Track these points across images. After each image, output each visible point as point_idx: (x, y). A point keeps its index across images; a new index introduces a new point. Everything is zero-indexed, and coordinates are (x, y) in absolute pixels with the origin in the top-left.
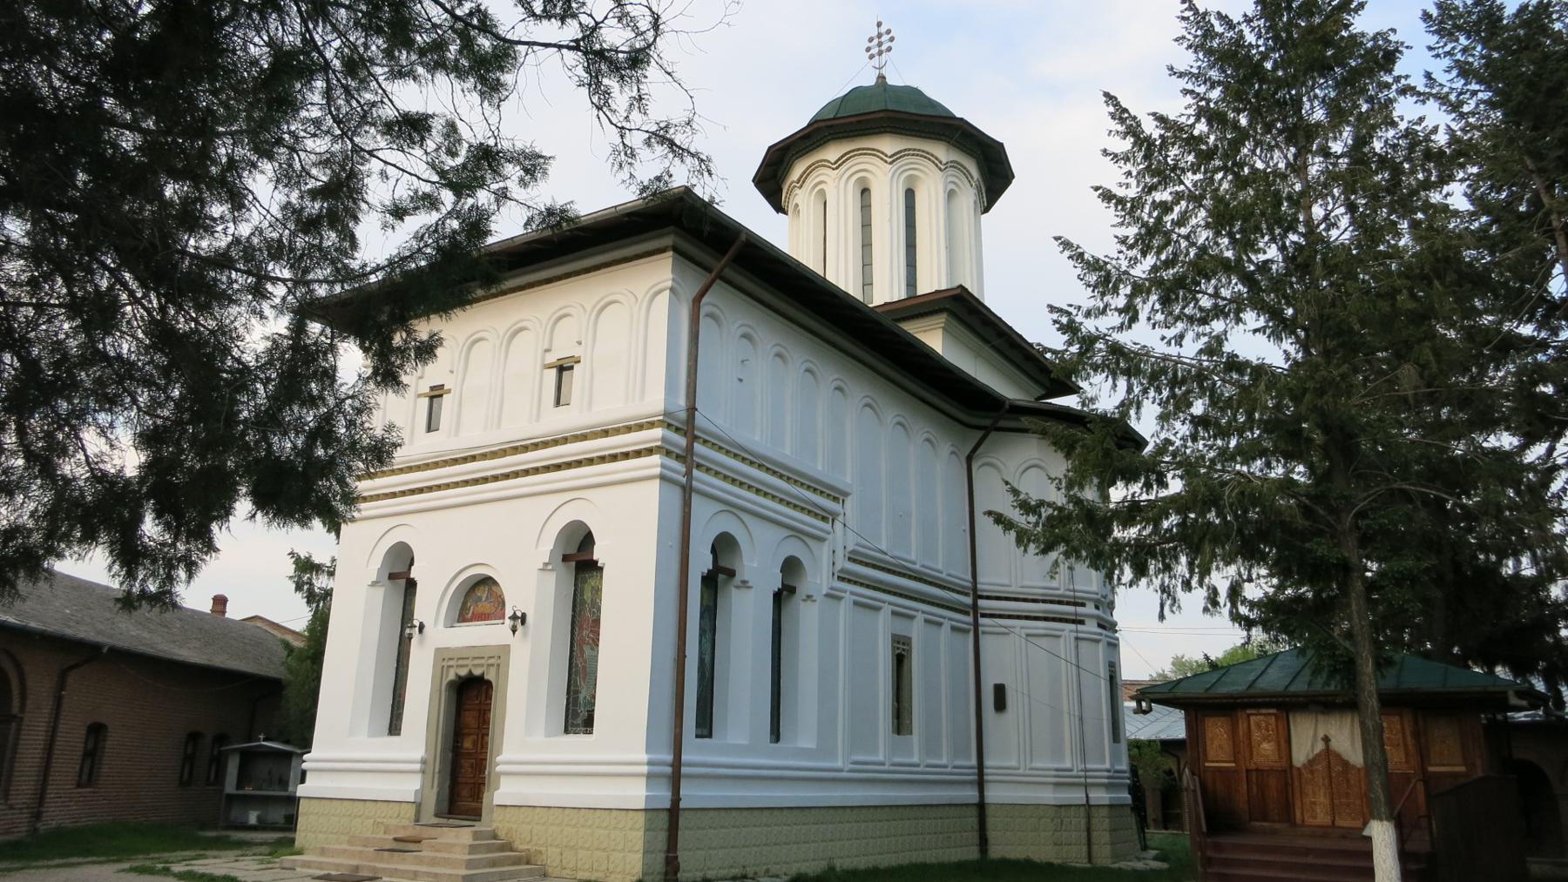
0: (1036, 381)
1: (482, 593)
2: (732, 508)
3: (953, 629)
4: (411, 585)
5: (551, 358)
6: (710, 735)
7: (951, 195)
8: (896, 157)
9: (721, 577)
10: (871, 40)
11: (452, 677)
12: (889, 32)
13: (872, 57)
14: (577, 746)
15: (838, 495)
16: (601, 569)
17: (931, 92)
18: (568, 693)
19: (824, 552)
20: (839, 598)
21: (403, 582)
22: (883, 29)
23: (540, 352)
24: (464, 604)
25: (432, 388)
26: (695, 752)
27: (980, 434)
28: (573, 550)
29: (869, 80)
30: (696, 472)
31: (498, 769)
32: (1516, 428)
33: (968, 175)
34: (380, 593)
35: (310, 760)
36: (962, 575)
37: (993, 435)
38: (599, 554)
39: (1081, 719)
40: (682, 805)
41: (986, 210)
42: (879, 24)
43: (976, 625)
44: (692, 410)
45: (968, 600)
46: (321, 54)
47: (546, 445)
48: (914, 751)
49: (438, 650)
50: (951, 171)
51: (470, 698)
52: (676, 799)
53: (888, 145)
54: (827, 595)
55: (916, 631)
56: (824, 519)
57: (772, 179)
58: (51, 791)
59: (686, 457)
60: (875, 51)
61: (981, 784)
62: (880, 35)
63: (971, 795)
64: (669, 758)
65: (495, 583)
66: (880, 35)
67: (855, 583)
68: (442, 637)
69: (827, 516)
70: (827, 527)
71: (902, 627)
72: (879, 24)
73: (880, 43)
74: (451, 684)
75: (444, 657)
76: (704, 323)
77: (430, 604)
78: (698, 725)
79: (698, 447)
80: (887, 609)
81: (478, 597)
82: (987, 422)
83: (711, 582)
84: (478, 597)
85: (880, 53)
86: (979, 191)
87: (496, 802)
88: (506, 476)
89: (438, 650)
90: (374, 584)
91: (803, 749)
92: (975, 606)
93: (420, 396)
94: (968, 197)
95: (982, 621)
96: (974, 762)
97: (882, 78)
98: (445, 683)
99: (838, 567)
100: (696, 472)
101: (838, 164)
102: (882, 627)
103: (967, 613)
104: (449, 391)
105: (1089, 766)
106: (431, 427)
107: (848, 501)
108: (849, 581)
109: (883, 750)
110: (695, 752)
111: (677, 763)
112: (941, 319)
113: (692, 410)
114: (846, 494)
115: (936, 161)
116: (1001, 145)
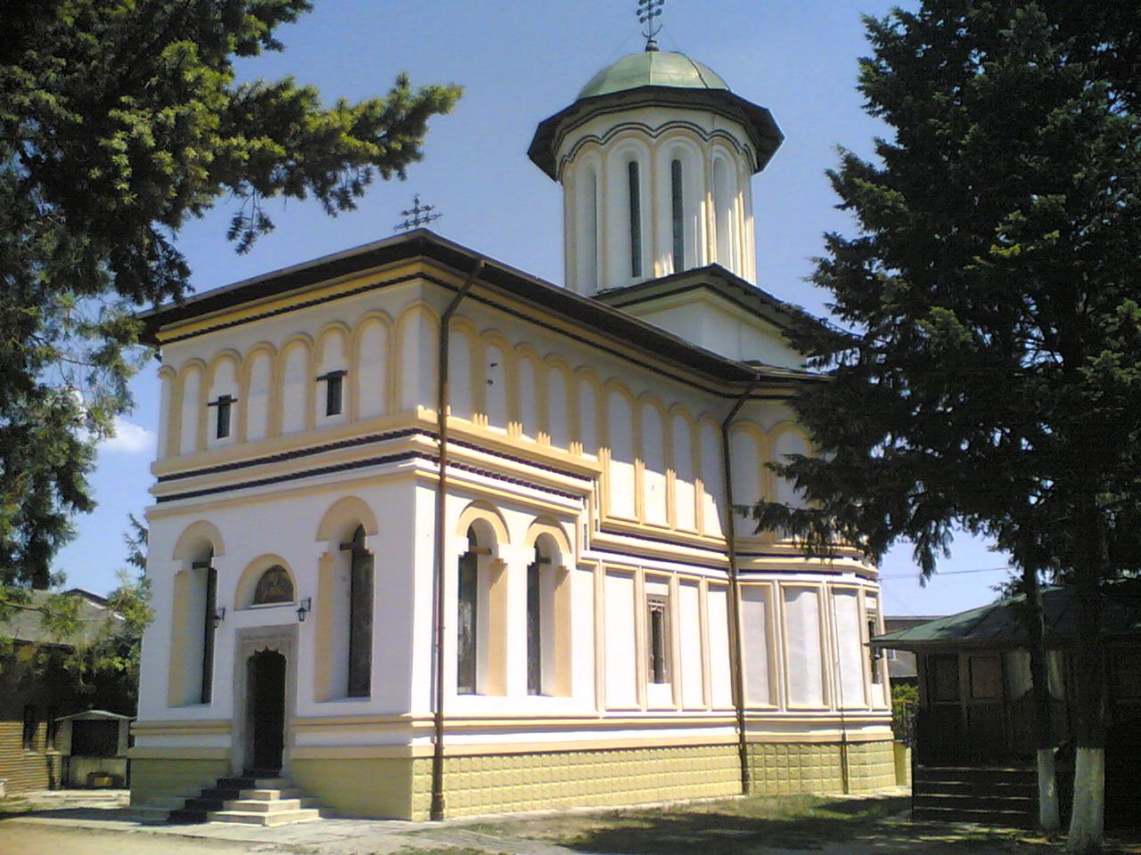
2: (482, 500)
4: (212, 575)
5: (323, 371)
13: (642, 20)
14: (658, 695)
21: (204, 570)
26: (457, 705)
27: (733, 402)
32: (882, 282)
38: (369, 543)
40: (445, 753)
46: (871, 274)
51: (267, 673)
52: (438, 747)
58: (747, 304)
60: (645, 14)
65: (284, 570)
68: (242, 621)
70: (578, 504)
74: (251, 659)
75: (244, 636)
77: (225, 594)
78: (459, 684)
79: (450, 447)
81: (273, 585)
83: (468, 563)
84: (273, 585)
85: (650, 16)
100: (449, 470)
106: (222, 431)
116: (765, 111)
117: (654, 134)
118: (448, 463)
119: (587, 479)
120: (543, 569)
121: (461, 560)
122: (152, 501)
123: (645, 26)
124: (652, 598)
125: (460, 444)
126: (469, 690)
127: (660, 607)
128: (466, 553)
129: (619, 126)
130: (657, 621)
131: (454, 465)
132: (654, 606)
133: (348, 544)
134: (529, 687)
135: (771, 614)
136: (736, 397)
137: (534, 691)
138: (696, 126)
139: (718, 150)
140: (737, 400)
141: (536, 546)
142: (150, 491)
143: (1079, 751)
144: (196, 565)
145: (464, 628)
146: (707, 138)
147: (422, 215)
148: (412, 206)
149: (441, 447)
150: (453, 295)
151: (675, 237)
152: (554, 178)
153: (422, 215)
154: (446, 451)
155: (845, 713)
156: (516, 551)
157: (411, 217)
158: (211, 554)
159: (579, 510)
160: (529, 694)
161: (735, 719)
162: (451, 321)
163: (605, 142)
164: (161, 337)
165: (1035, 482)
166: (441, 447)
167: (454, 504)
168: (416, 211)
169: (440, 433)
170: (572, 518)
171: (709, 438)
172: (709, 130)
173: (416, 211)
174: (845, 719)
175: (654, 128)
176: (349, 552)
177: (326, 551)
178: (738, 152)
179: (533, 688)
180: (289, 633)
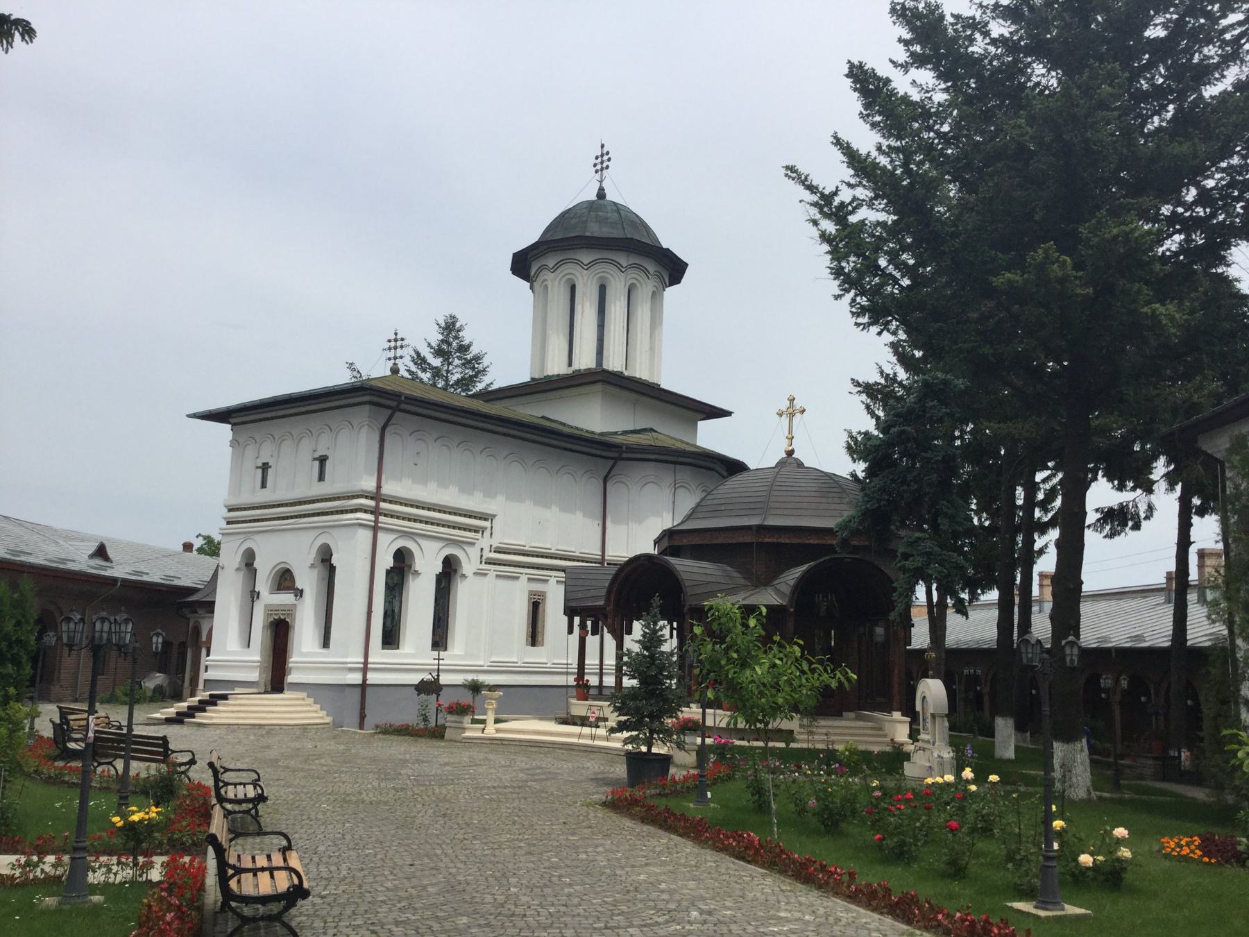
5: (317, 455)
19: (474, 552)
26: (379, 655)
27: (611, 462)
33: (646, 271)
37: (620, 463)
38: (334, 561)
42: (603, 146)
44: (379, 487)
48: (538, 656)
50: (632, 271)
52: (365, 679)
53: (586, 257)
54: (475, 574)
59: (376, 512)
62: (602, 155)
63: (356, 678)
66: (602, 155)
68: (270, 599)
70: (478, 536)
72: (603, 146)
75: (269, 609)
76: (387, 441)
77: (263, 585)
81: (285, 580)
82: (616, 455)
85: (602, 169)
88: (296, 517)
90: (238, 569)
97: (601, 194)
100: (381, 519)
111: (366, 663)
113: (379, 487)
114: (495, 516)
115: (618, 266)
118: (380, 514)
119: (486, 519)
121: (388, 572)
123: (598, 176)
124: (532, 593)
131: (386, 515)
139: (634, 275)
143: (1055, 744)
144: (323, 561)
147: (399, 343)
148: (393, 337)
150: (389, 412)
153: (399, 343)
156: (428, 563)
157: (393, 344)
165: (969, 504)
166: (377, 505)
168: (396, 340)
169: (377, 496)
171: (597, 485)
173: (396, 340)
180: (291, 610)
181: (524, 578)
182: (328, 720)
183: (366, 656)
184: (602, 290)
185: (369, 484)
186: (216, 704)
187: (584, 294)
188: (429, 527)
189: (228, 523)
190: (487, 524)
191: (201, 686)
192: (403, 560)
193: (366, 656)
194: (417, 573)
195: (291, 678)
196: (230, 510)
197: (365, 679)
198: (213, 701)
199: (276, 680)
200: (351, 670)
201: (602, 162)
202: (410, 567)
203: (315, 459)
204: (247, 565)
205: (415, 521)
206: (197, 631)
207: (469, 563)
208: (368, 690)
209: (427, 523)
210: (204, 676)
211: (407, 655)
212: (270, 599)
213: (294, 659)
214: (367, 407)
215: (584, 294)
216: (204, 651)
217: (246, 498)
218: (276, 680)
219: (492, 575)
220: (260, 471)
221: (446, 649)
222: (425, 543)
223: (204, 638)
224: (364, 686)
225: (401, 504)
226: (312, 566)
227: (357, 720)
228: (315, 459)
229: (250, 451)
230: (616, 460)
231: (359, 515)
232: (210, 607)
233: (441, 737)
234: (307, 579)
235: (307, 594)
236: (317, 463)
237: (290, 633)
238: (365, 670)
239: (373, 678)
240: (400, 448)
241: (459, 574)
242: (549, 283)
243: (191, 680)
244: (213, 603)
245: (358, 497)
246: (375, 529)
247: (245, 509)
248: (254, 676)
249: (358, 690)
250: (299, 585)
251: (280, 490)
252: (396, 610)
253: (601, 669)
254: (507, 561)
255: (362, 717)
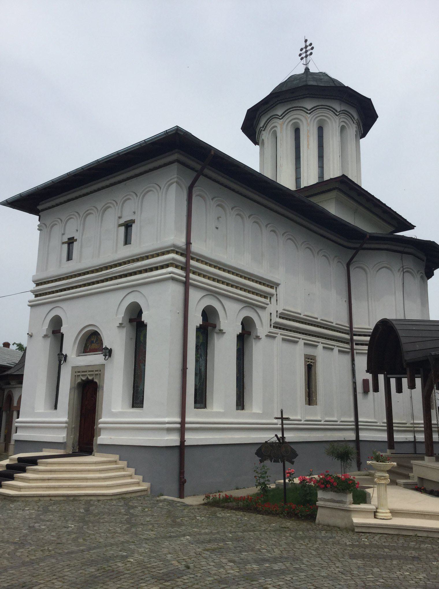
0: (389, 223)
1: (94, 339)
3: (340, 351)
5: (122, 221)
6: (243, 409)
7: (343, 129)
8: (314, 109)
9: (209, 328)
10: (301, 50)
11: (79, 381)
12: (311, 44)
13: (302, 59)
14: (136, 416)
15: (273, 285)
16: (146, 326)
17: (333, 75)
18: (134, 388)
19: (265, 315)
20: (274, 337)
22: (308, 43)
23: (117, 218)
24: (86, 345)
25: (69, 239)
26: (193, 416)
27: (354, 251)
28: (135, 316)
29: (300, 70)
30: (191, 275)
31: (100, 426)
33: (352, 117)
34: (49, 341)
35: (17, 422)
36: (345, 323)
38: (145, 318)
39: (411, 397)
40: (186, 444)
41: (363, 135)
42: (306, 41)
43: (352, 349)
44: (188, 243)
45: (348, 337)
47: (120, 264)
49: (72, 367)
50: (342, 116)
52: (183, 440)
54: (267, 336)
55: (319, 352)
56: (265, 297)
57: (253, 124)
59: (186, 268)
61: (357, 430)
62: (306, 47)
63: (173, 440)
64: (179, 420)
65: (99, 334)
66: (306, 47)
67: (283, 329)
68: (77, 360)
69: (265, 295)
70: (267, 301)
71: (310, 351)
72: (306, 41)
73: (307, 51)
74: (79, 384)
75: (76, 371)
77: (70, 347)
79: (192, 262)
80: (301, 342)
81: (92, 341)
82: (358, 245)
85: (306, 56)
86: (358, 125)
87: (99, 442)
89: (72, 367)
90: (45, 336)
91: (254, 413)
92: (352, 339)
93: (63, 243)
94: (352, 130)
95: (355, 347)
96: (353, 419)
97: (307, 70)
98: (77, 383)
99: (273, 322)
100: (191, 275)
101: (283, 116)
102: (298, 352)
103: (347, 343)
104: (76, 240)
105: (416, 422)
107: (280, 289)
108: (280, 328)
109: (299, 412)
110: (193, 416)
111: (183, 423)
112: (334, 194)
113: (188, 243)
114: (278, 285)
115: (334, 111)
117: (309, 112)
119: (272, 287)
120: (245, 335)
122: (32, 297)
125: (198, 260)
126: (203, 405)
127: (311, 362)
128: (200, 325)
129: (290, 109)
130: (310, 369)
131: (194, 273)
132: (308, 362)
133: (135, 319)
134: (237, 405)
135: (80, 490)
136: (354, 248)
137: (240, 407)
138: (332, 108)
140: (355, 251)
141: (242, 324)
142: (33, 292)
145: (200, 370)
146: (338, 114)
149: (187, 262)
151: (323, 147)
152: (256, 143)
154: (189, 264)
155: (415, 425)
156: (230, 323)
158: (140, 312)
159: (268, 304)
160: (237, 409)
161: (353, 427)
162: (194, 189)
163: (282, 118)
164: (40, 207)
166: (187, 262)
167: (194, 295)
170: (264, 308)
172: (339, 110)
174: (415, 429)
175: (309, 108)
176: (135, 323)
177: (121, 322)
178: (354, 123)
179: (240, 405)
180: (100, 370)
181: (301, 342)
182: (145, 486)
183: (183, 415)
184: (320, 130)
185: (181, 241)
186: (24, 471)
187: (308, 131)
188: (229, 288)
189: (36, 296)
190: (273, 291)
191: (11, 448)
192: (209, 314)
193: (183, 415)
194: (221, 332)
195: (103, 438)
196: (38, 285)
197: (183, 440)
198: (23, 465)
199: (84, 438)
200: (169, 430)
201: (307, 51)
202: (214, 326)
203: (120, 225)
204: (54, 332)
205: (218, 281)
206: (10, 398)
207: (262, 328)
208: (187, 452)
209: (228, 284)
210: (15, 436)
211: (218, 414)
212: (77, 360)
213: (104, 419)
214: (175, 166)
215: (308, 131)
216: (15, 414)
217: (53, 271)
218: (84, 438)
219: (279, 337)
220: (66, 246)
221: (205, 407)
222: (228, 304)
223: (15, 404)
224: (182, 448)
225: (206, 264)
226: (121, 326)
227: (175, 486)
228: (120, 225)
229: (57, 230)
230: (357, 250)
231: (170, 269)
232: (19, 379)
233: (311, 517)
234: (116, 338)
235: (115, 353)
236: (122, 229)
237: (99, 394)
238: (182, 430)
239: (191, 438)
240: (205, 213)
241: (253, 335)
242: (278, 130)
243: (5, 436)
244: (23, 375)
245: (168, 252)
246: (187, 285)
247: (52, 281)
248: (61, 436)
249: (177, 453)
250: (106, 344)
251: (86, 258)
252: (203, 369)
253: (357, 425)
254: (293, 326)
255: (182, 482)
